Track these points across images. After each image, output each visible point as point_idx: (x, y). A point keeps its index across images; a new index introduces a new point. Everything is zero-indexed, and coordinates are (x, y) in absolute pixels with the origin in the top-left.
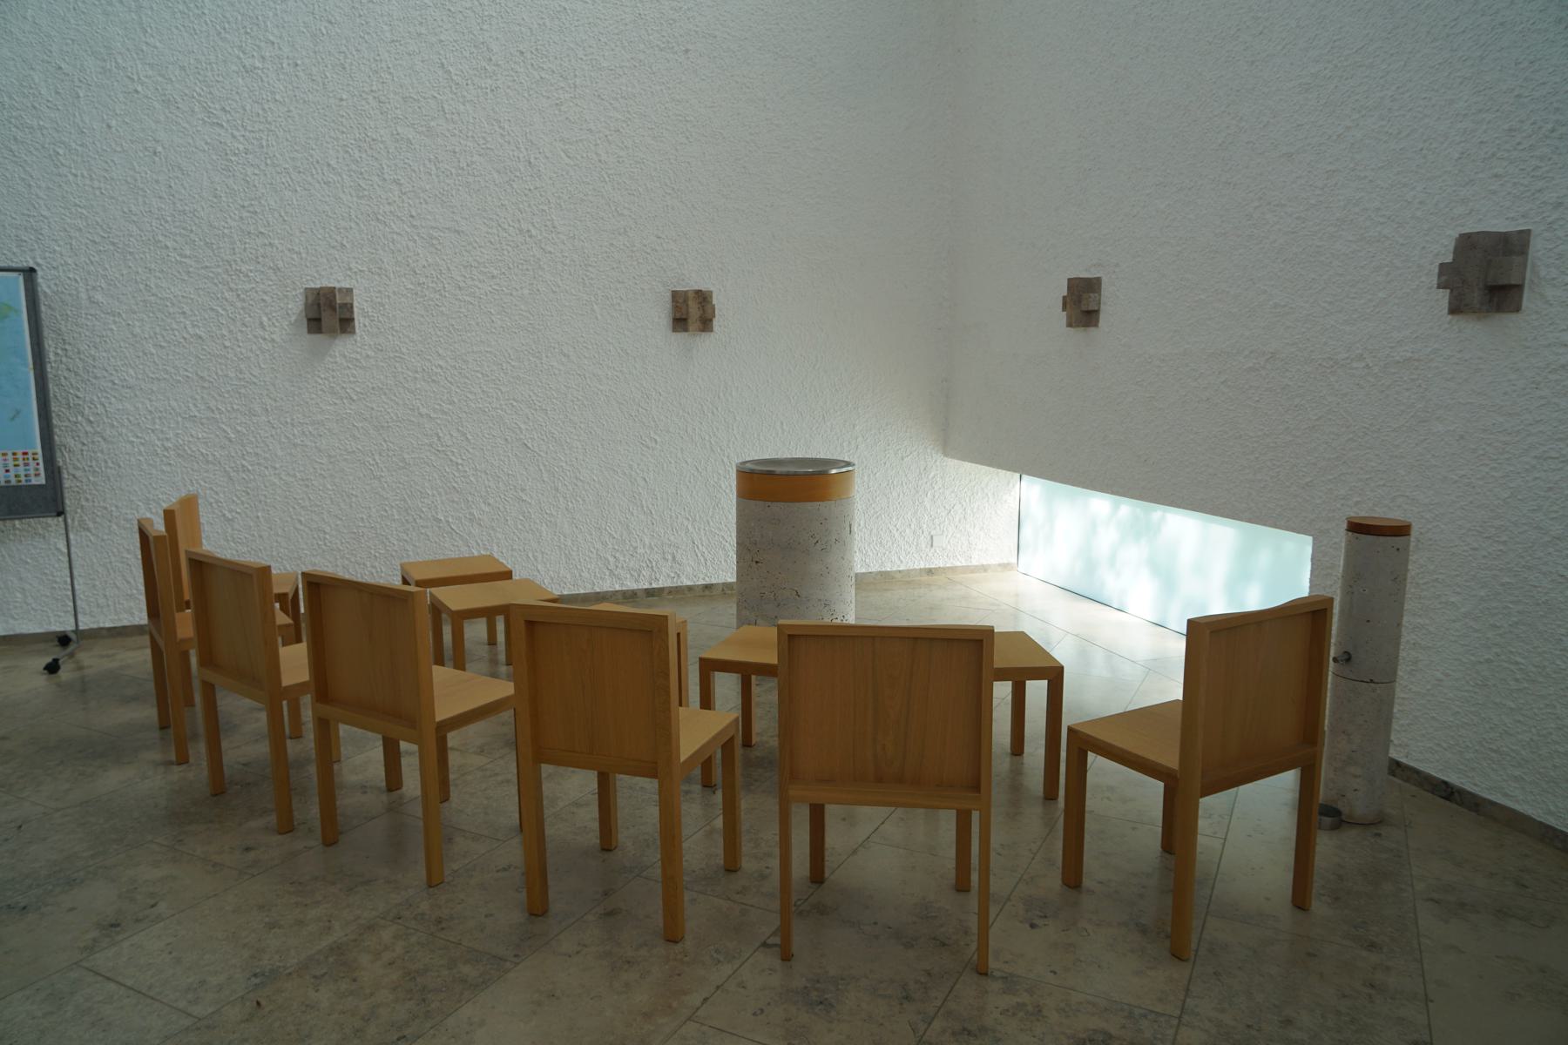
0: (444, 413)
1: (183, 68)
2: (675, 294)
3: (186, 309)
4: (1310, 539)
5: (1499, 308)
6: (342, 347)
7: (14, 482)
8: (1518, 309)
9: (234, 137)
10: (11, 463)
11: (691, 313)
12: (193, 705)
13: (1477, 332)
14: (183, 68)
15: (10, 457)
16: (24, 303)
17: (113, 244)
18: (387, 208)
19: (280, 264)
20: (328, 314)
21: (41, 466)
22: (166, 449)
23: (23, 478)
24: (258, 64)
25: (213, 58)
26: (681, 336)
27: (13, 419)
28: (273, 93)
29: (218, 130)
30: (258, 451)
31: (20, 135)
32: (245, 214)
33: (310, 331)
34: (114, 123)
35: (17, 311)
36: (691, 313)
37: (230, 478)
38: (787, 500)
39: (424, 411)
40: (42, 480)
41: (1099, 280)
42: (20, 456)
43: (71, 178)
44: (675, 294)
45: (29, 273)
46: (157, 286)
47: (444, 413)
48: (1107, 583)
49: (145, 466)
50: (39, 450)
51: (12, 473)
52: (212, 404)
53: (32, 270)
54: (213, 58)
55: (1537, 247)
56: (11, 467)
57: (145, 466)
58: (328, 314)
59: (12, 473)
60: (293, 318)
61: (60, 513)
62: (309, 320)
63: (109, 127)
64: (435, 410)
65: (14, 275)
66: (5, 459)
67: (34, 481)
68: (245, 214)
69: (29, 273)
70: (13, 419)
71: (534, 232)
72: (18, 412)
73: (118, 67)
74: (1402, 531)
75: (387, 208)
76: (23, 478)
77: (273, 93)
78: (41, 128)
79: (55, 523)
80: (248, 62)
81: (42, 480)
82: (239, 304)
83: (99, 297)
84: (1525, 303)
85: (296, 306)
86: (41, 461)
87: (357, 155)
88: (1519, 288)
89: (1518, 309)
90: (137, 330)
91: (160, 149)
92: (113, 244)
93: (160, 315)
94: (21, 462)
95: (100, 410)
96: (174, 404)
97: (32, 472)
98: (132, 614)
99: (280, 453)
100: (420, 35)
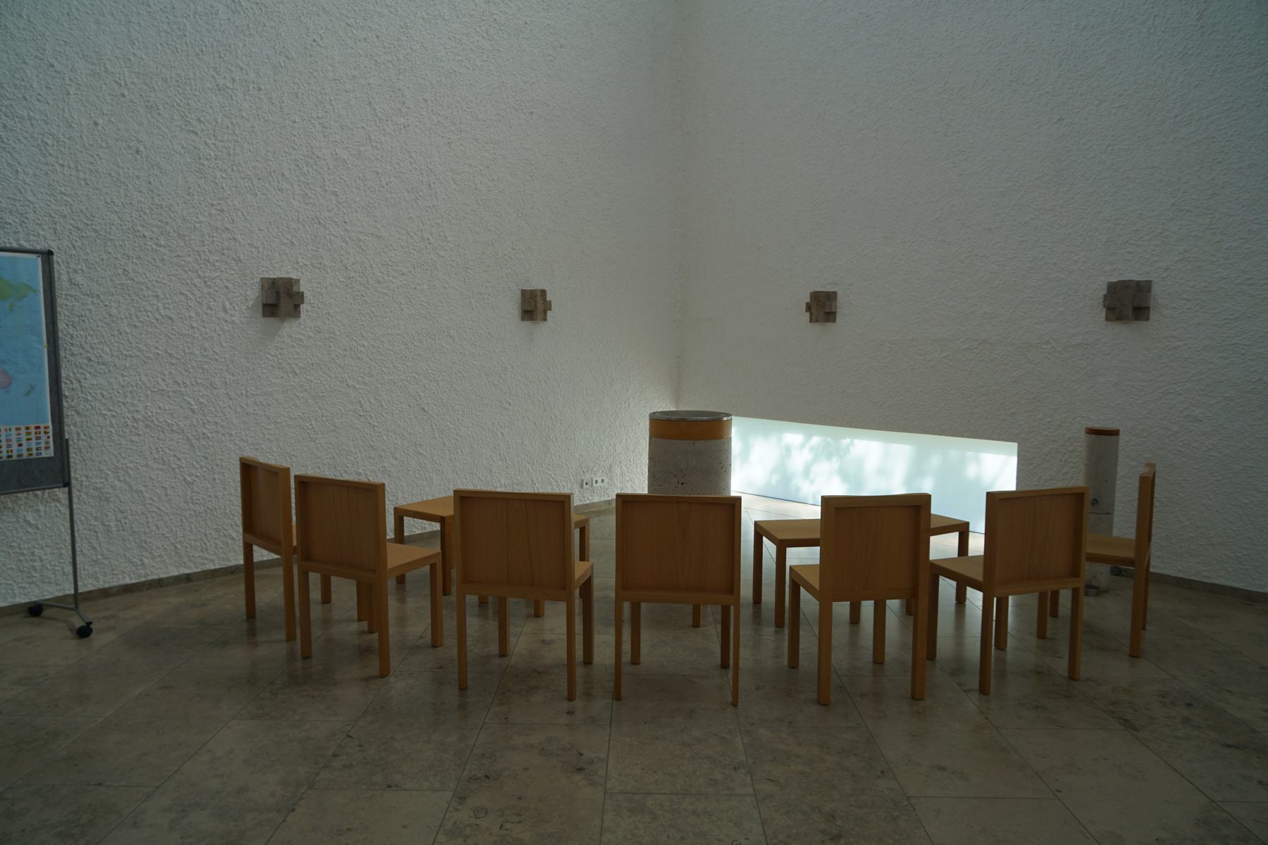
0: (365, 384)
1: (165, 80)
2: (523, 292)
3: (159, 292)
4: (1014, 446)
5: (827, 321)
6: (289, 329)
7: (25, 455)
8: (1148, 319)
9: (206, 144)
10: (24, 437)
11: (533, 306)
12: (295, 639)
13: (1122, 331)
14: (165, 80)
15: (23, 431)
16: (41, 284)
17: (95, 231)
18: (327, 214)
19: (242, 257)
20: (280, 300)
21: (51, 440)
22: (136, 420)
23: (34, 452)
24: (230, 85)
25: (191, 74)
26: (528, 324)
27: (28, 394)
28: (240, 110)
29: (193, 137)
30: (218, 420)
31: (9, 123)
32: (214, 212)
33: (265, 315)
34: (100, 121)
35: (36, 291)
36: (533, 306)
37: (192, 445)
38: (690, 441)
39: (351, 382)
40: (51, 453)
41: (835, 293)
42: (33, 430)
43: (58, 167)
44: (523, 292)
45: (47, 255)
46: (134, 271)
47: (365, 384)
48: (971, 475)
49: (115, 438)
50: (50, 424)
51: (24, 448)
52: (179, 379)
53: (50, 253)
54: (191, 74)
55: (1156, 289)
56: (24, 442)
57: (115, 438)
58: (822, 307)
59: (24, 448)
60: (251, 303)
61: (67, 484)
62: (265, 305)
63: (96, 124)
64: (358, 382)
65: (33, 256)
66: (13, 432)
67: (44, 454)
68: (214, 212)
69: (47, 255)
70: (28, 394)
71: (432, 240)
72: (32, 388)
73: (107, 72)
74: (1115, 433)
75: (327, 214)
76: (34, 452)
77: (240, 110)
78: (30, 118)
79: (61, 493)
80: (221, 82)
81: (51, 453)
82: (205, 290)
83: (79, 279)
84: (1151, 317)
85: (253, 293)
86: (51, 435)
87: (305, 169)
88: (1148, 308)
89: (1148, 319)
90: (114, 311)
91: (142, 149)
92: (95, 231)
93: (134, 297)
94: (33, 436)
95: (76, 385)
96: (144, 379)
97: (43, 445)
98: (97, 579)
99: (235, 422)
100: (354, 77)
